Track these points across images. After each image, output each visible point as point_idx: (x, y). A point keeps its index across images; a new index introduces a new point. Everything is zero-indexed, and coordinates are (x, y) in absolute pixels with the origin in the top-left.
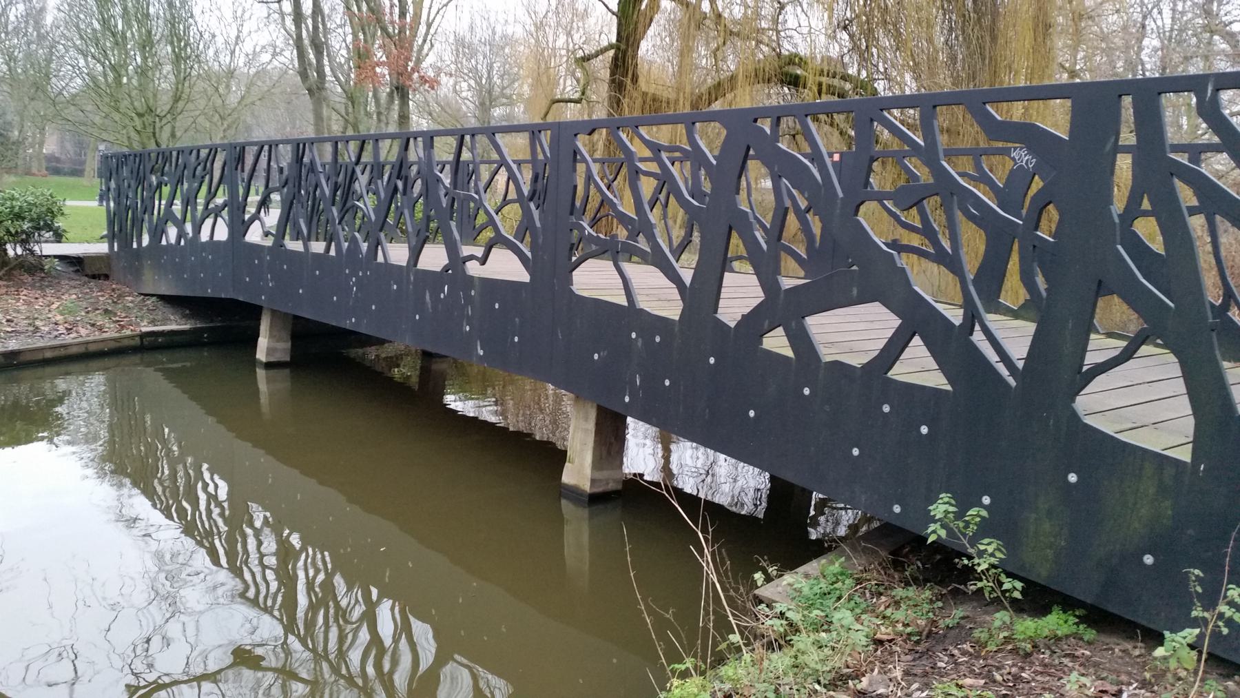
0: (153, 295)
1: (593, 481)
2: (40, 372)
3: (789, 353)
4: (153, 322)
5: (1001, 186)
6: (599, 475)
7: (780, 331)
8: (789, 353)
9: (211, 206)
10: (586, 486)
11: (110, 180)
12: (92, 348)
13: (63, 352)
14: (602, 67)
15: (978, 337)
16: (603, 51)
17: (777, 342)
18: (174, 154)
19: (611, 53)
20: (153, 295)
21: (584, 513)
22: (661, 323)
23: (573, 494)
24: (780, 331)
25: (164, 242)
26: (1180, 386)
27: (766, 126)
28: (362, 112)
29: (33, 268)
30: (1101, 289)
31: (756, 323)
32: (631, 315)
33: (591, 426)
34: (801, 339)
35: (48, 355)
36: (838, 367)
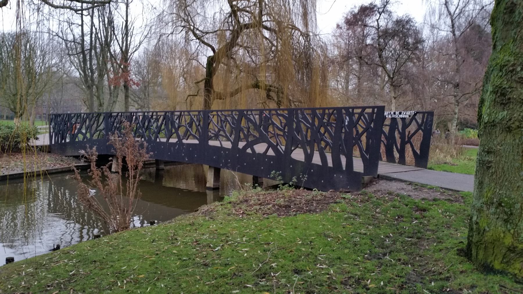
0: (71, 156)
1: (214, 185)
2: (63, 174)
3: (251, 152)
4: (76, 163)
5: (196, 142)
6: (215, 184)
7: (249, 149)
8: (251, 152)
9: (98, 129)
10: (212, 186)
11: (52, 122)
12: (64, 170)
13: (57, 171)
14: (202, 85)
15: (279, 147)
16: (202, 81)
17: (249, 151)
18: (83, 115)
19: (204, 81)
20: (71, 156)
21: (212, 192)
22: (228, 149)
23: (209, 189)
24: (249, 149)
25: (77, 140)
26: (354, 165)
27: (245, 112)
28: (101, 92)
29: (29, 149)
30: (321, 140)
31: (245, 148)
32: (222, 148)
33: (213, 173)
34: (253, 150)
35: (54, 171)
36: (259, 154)
